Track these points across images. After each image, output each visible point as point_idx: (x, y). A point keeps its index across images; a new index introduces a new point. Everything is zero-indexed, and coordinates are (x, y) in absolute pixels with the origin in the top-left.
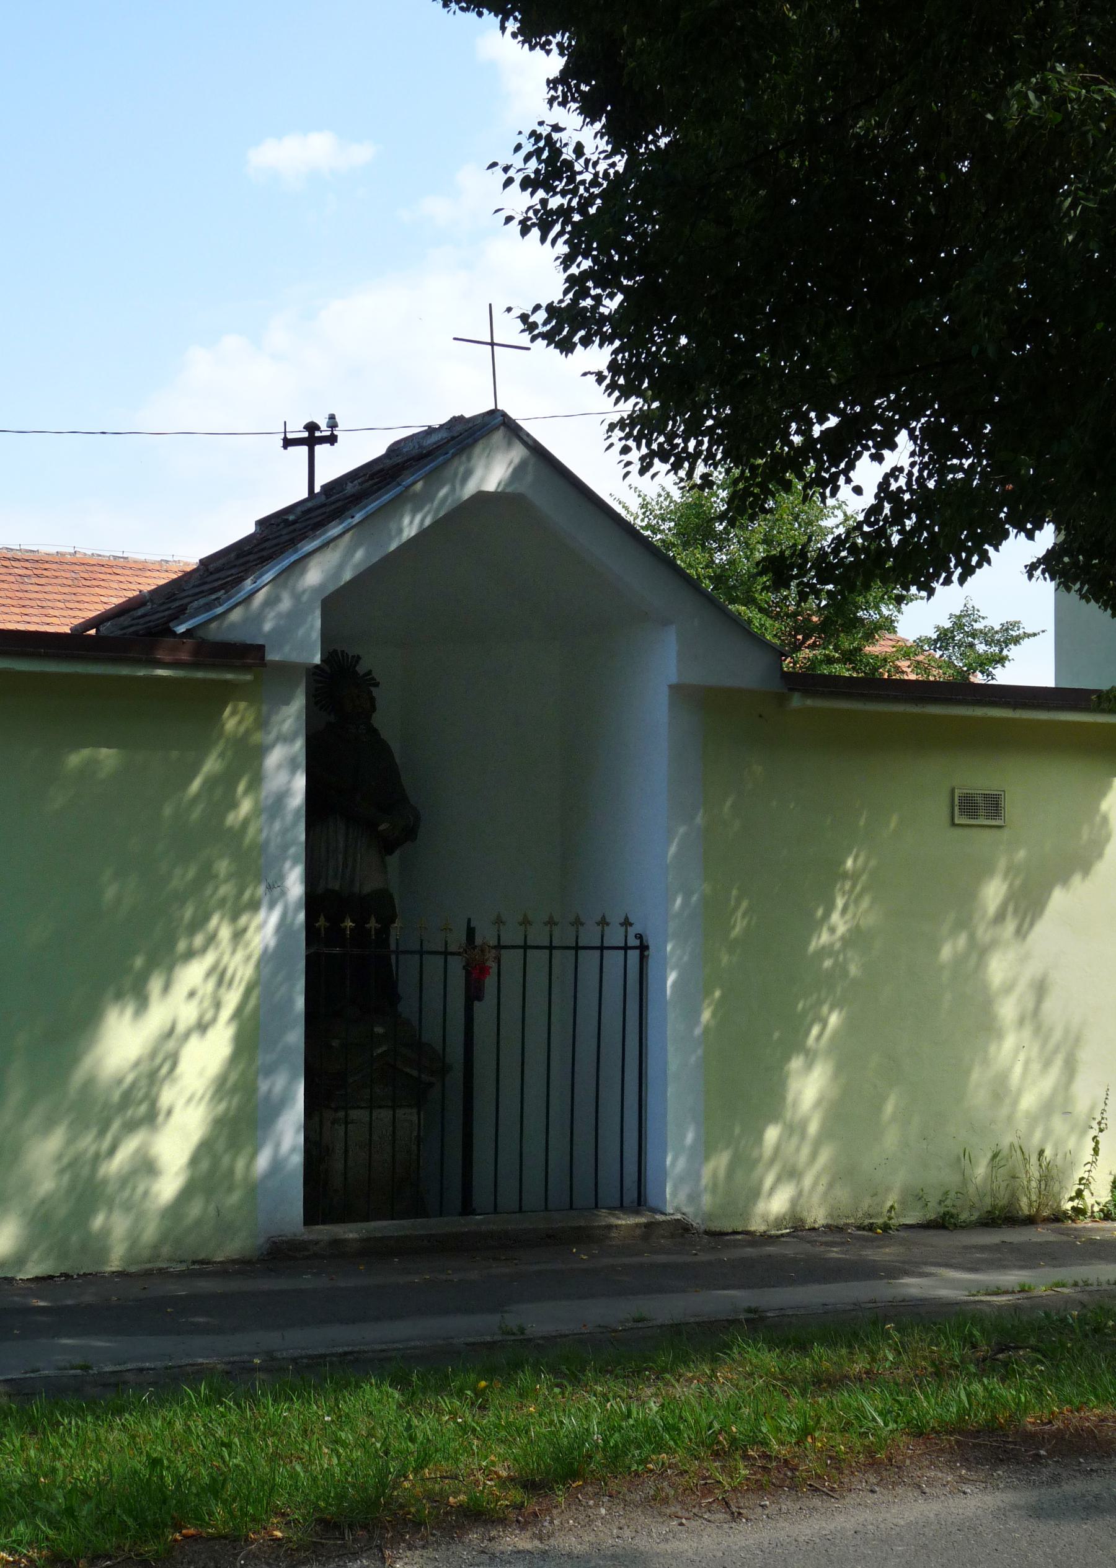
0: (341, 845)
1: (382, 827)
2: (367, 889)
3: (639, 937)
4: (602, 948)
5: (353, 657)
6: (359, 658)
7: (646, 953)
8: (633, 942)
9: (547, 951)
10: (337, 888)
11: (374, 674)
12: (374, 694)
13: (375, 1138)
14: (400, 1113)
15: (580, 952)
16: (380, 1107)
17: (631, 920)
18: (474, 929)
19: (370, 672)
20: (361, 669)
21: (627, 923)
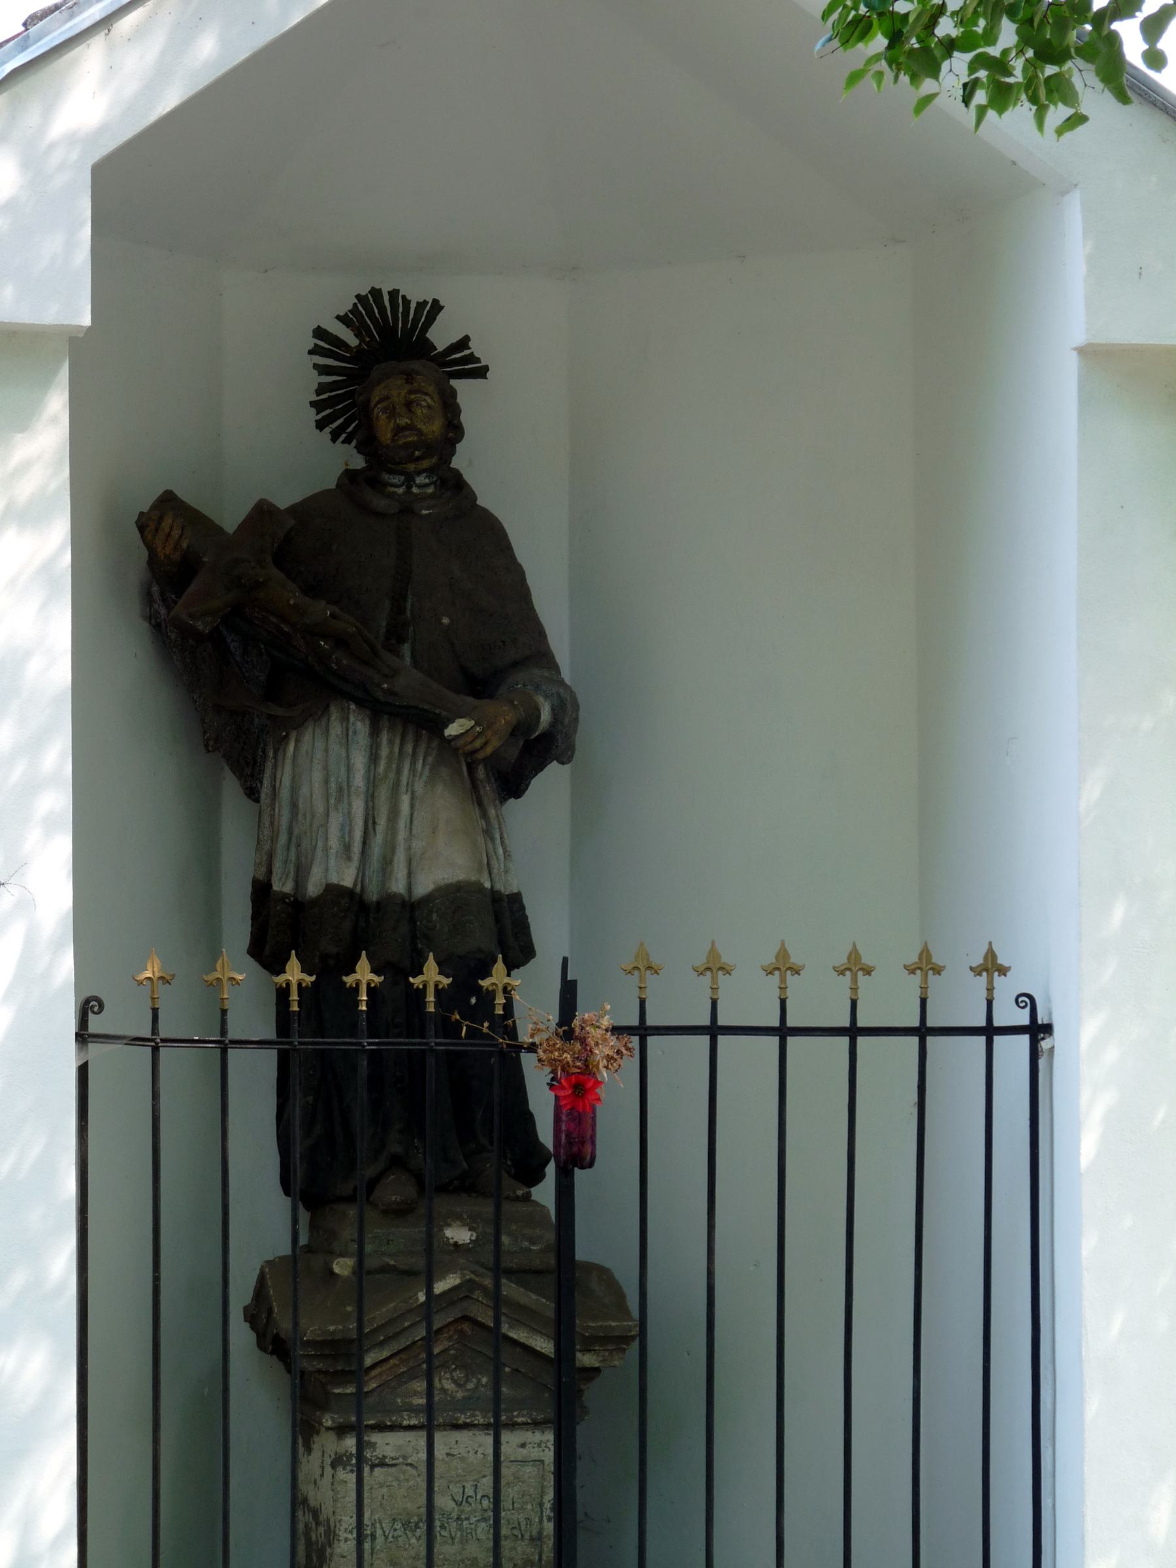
0: (359, 781)
1: (453, 730)
2: (424, 886)
3: (1028, 1001)
4: (923, 1032)
5: (421, 305)
6: (437, 307)
7: (1045, 1045)
8: (1009, 1014)
9: (914, 1041)
10: (348, 882)
11: (475, 348)
12: (461, 400)
13: (443, 1502)
14: (510, 1439)
15: (931, 1040)
16: (457, 1427)
17: (937, 959)
18: (574, 983)
19: (464, 343)
20: (441, 336)
21: (991, 967)
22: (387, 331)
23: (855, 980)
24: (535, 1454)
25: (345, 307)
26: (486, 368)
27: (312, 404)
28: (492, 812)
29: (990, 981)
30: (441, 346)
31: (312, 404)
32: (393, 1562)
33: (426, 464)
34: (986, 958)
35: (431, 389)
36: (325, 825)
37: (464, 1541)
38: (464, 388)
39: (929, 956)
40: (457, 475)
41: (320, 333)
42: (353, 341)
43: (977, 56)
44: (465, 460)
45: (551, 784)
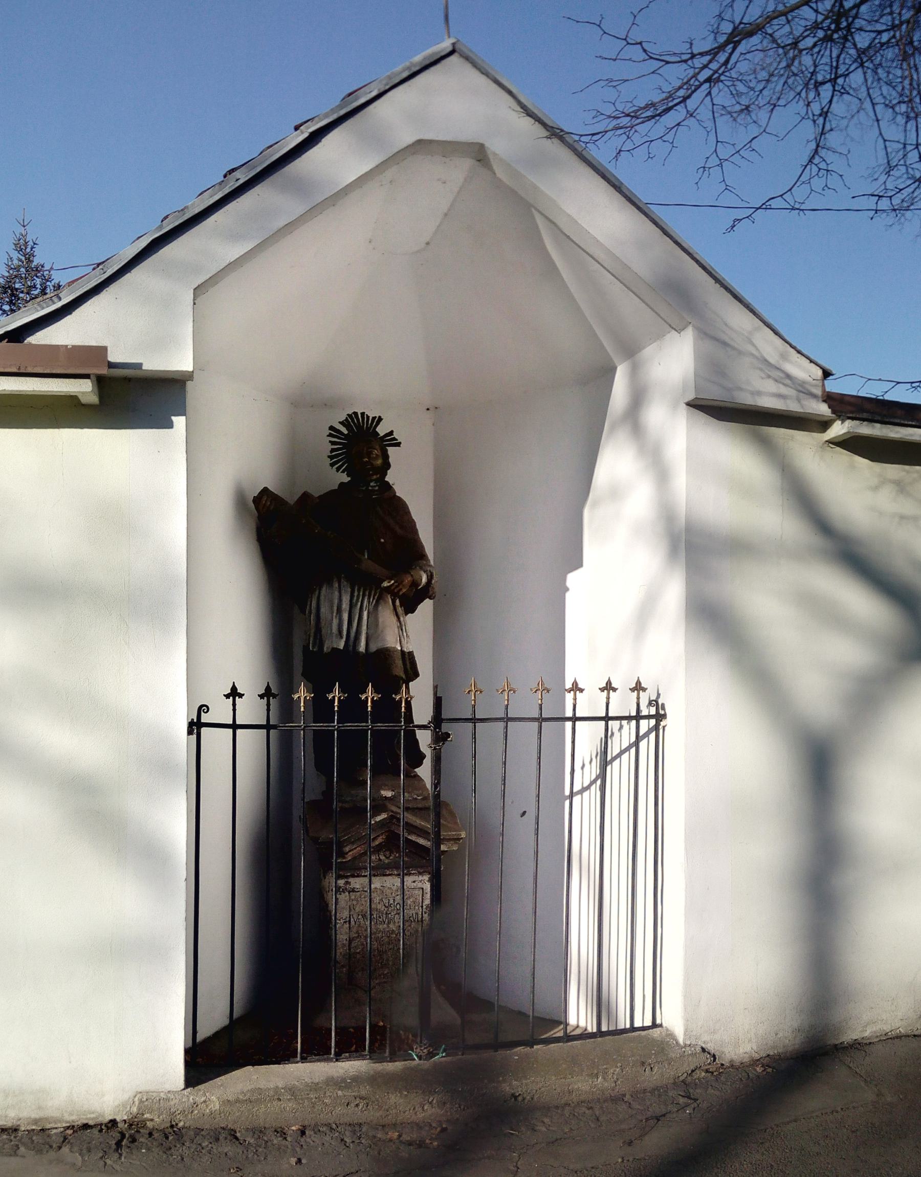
5: (374, 418)
6: (380, 419)
11: (395, 435)
12: (389, 453)
19: (391, 433)
20: (382, 430)
22: (359, 426)
23: (609, 694)
24: (420, 885)
25: (343, 418)
26: (400, 443)
27: (329, 457)
28: (402, 619)
29: (638, 695)
30: (382, 434)
31: (329, 457)
32: (264, 1175)
33: (375, 477)
34: (232, 689)
35: (377, 447)
36: (331, 624)
37: (389, 923)
38: (391, 450)
39: (610, 684)
40: (388, 483)
41: (331, 428)
42: (346, 432)
43: (424, 756)
44: (391, 477)
45: (426, 607)
